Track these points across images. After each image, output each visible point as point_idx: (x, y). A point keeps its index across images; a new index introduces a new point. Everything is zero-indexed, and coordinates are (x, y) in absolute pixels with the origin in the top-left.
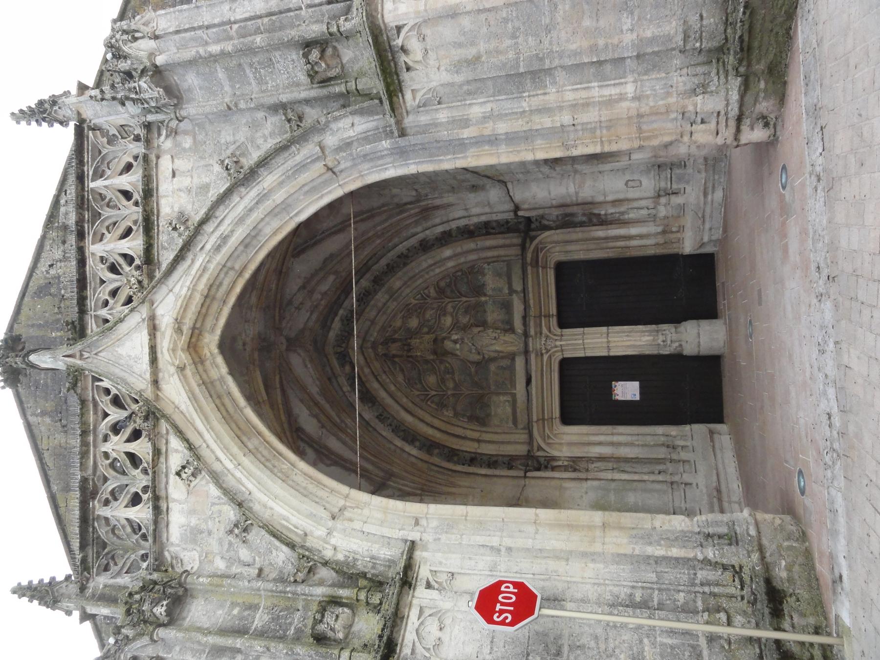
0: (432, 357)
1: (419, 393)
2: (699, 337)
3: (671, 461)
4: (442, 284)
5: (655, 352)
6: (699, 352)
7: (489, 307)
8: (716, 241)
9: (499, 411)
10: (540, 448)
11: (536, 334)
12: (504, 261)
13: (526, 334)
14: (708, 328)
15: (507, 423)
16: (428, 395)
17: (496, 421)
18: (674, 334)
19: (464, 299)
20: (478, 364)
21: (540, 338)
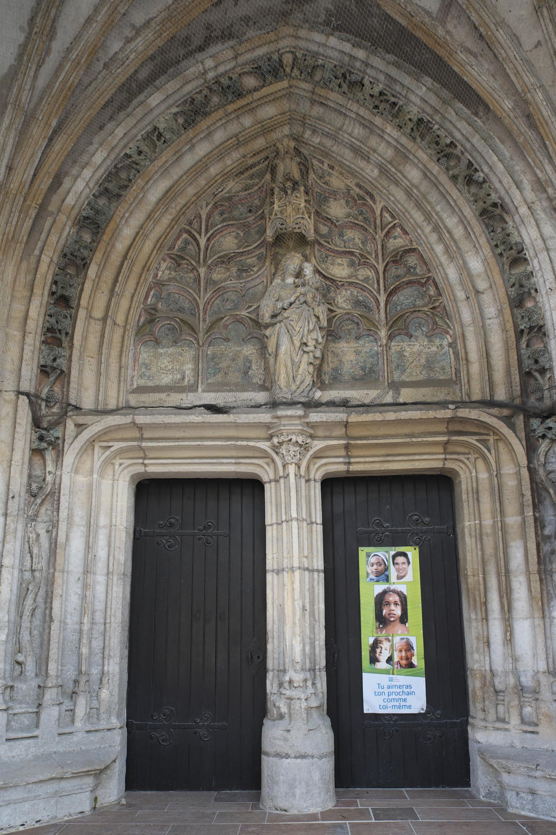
1: (204, 217)
2: (296, 757)
5: (270, 664)
6: (267, 754)
8: (502, 796)
10: (80, 427)
11: (312, 425)
12: (458, 371)
14: (316, 776)
16: (200, 235)
17: (145, 355)
18: (304, 705)
19: (382, 299)
21: (302, 433)
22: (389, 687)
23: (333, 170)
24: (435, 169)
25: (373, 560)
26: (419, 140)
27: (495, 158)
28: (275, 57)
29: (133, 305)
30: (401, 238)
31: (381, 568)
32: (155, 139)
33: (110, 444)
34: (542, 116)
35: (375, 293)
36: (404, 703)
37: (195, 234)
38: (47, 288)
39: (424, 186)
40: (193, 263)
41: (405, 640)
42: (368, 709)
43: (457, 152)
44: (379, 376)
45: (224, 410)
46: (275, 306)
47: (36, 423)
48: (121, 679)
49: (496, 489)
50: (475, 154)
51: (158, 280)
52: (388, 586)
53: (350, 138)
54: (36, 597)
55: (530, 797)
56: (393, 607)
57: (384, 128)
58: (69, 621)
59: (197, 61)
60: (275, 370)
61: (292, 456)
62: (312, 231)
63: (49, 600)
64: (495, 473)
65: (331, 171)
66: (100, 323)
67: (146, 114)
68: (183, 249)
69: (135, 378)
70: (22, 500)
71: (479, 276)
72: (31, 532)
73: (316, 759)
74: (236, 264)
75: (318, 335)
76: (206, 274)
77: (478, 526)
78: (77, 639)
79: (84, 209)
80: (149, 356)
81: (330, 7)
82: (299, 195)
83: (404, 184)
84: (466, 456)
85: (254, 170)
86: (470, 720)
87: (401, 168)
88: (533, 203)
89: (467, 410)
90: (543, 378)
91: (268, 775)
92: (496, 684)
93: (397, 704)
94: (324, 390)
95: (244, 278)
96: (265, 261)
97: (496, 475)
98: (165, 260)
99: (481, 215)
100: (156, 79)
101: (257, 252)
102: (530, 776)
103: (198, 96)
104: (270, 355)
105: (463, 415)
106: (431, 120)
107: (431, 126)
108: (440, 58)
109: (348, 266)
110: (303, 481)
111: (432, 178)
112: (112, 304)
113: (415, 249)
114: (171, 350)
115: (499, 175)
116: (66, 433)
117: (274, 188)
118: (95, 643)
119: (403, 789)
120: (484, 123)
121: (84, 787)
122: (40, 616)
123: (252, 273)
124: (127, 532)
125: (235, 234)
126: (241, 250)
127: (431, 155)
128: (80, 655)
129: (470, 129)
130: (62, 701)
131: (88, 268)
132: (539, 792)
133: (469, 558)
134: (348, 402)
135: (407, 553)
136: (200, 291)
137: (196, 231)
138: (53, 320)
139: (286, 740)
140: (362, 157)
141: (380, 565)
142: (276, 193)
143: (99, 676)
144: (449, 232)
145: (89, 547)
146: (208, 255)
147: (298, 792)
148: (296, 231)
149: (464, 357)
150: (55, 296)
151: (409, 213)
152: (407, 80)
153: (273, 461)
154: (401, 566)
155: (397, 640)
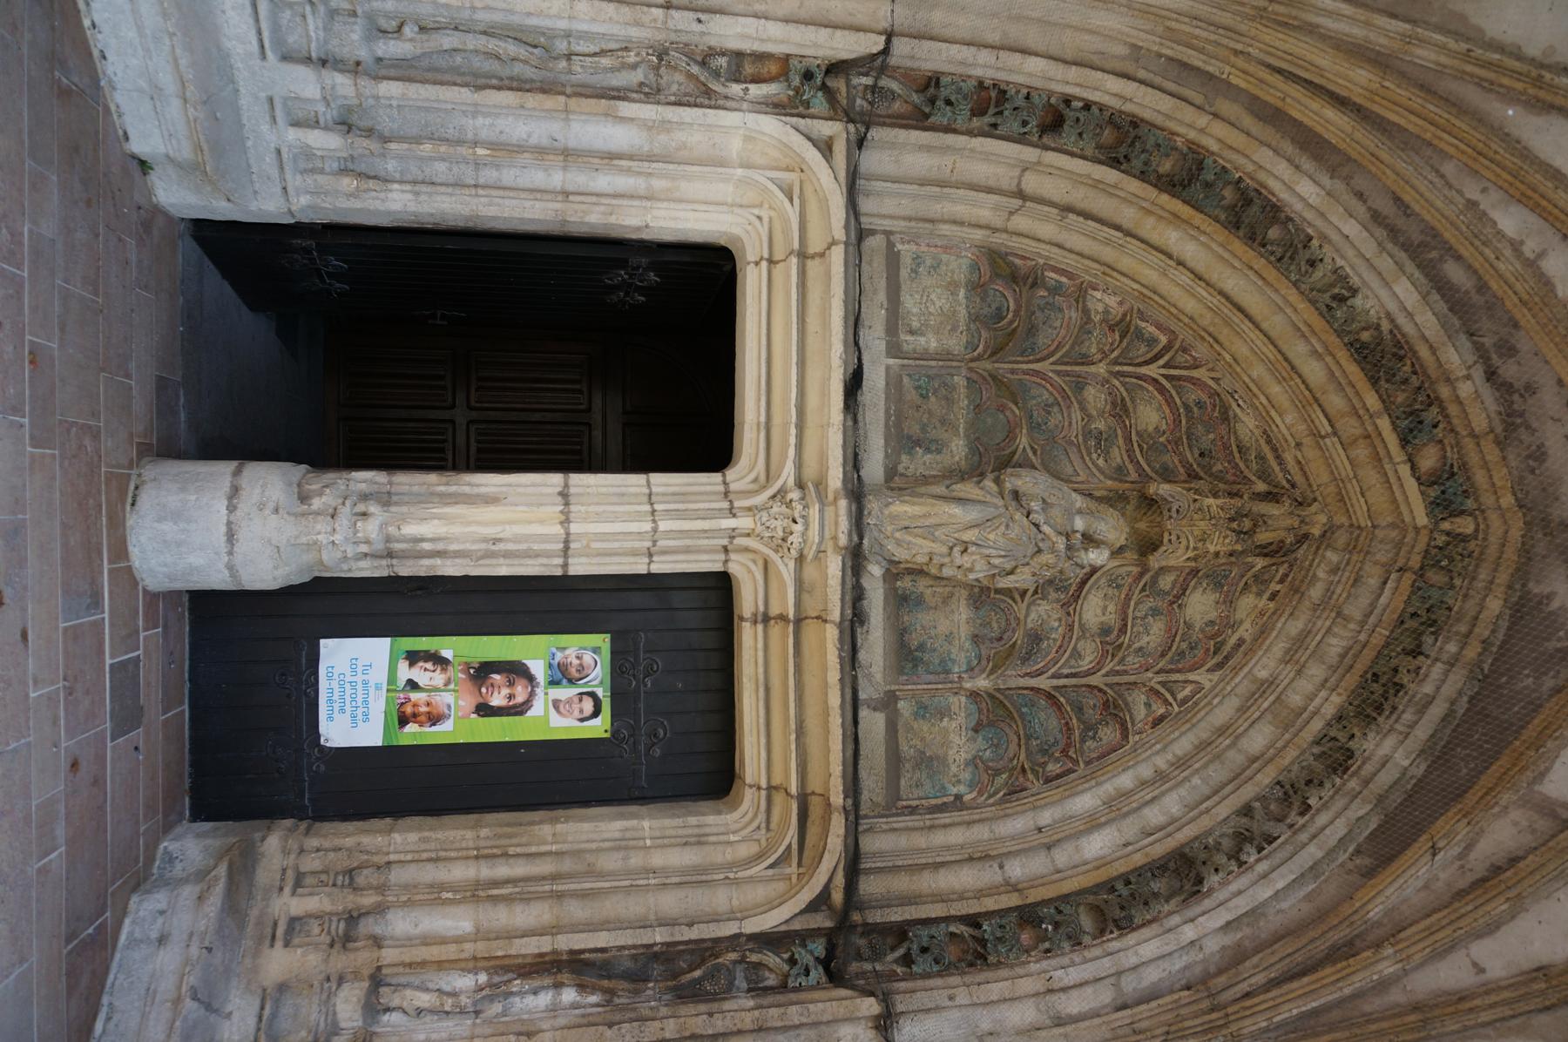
0: (1164, 489)
1: (1195, 373)
2: (229, 523)
3: (356, 68)
4: (1108, 734)
6: (237, 473)
7: (961, 653)
9: (940, 301)
10: (826, 147)
12: (913, 810)
13: (856, 559)
14: (197, 560)
15: (917, 259)
16: (1164, 367)
19: (1043, 683)
20: (1005, 463)
22: (365, 683)
23: (1269, 599)
24: (1266, 778)
25: (588, 658)
26: (1316, 750)
27: (1280, 885)
28: (1470, 504)
29: (1044, 246)
30: (1147, 716)
31: (574, 673)
32: (1336, 291)
33: (796, 201)
34: (1354, 973)
35: (1053, 670)
36: (336, 709)
37: (1166, 358)
38: (1076, 91)
39: (1235, 758)
40: (1115, 354)
41: (446, 711)
42: (327, 646)
43: (1293, 817)
44: (907, 674)
46: (1033, 497)
47: (837, 68)
48: (377, 212)
49: (704, 878)
50: (1289, 848)
51: (1086, 291)
52: (542, 683)
53: (1323, 631)
54: (521, 61)
55: (154, 935)
56: (505, 691)
57: (1339, 690)
58: (480, 121)
59: (1470, 367)
60: (922, 495)
61: (768, 524)
62: (1164, 563)
63: (515, 84)
64: (731, 875)
65: (1266, 595)
66: (1013, 187)
67: (1380, 274)
68: (1139, 334)
69: (914, 247)
70: (696, 39)
71: (1077, 849)
72: (638, 54)
73: (226, 559)
74: (1110, 428)
75: (980, 573)
76: (1095, 376)
77: (641, 843)
78: (447, 136)
79: (1215, 162)
80: (953, 272)
81: (1555, 604)
82: (1227, 541)
83: (1240, 721)
84: (763, 825)
85: (1273, 463)
86: (304, 825)
87: (1269, 717)
88: (1201, 948)
89: (842, 831)
90: (896, 961)
91: (199, 474)
92: (365, 872)
93: (336, 697)
94: (885, 581)
95: (1085, 441)
96: (1116, 479)
97: (727, 878)
98: (1121, 303)
99: (1183, 856)
100: (1439, 290)
101: (1130, 467)
102: (191, 935)
103: (1407, 368)
104: (947, 487)
105: (833, 822)
106: (1349, 772)
107: (1339, 772)
108: (1459, 795)
109: (1102, 623)
110: (725, 542)
111: (1248, 773)
112: (1046, 209)
113: (1127, 737)
114: (962, 313)
115: (1251, 891)
116: (815, 121)
117: (1241, 497)
118: (441, 167)
119: (186, 707)
120: (1342, 865)
121: (174, 142)
122: (488, 68)
123: (1094, 456)
124: (639, 229)
125: (1164, 427)
126: (1134, 438)
127: (1290, 771)
128: (417, 140)
129: (1332, 842)
130: (333, 105)
131: (1111, 167)
132: (162, 952)
133: (586, 826)
134: (862, 623)
135: (600, 717)
136: (1066, 364)
137: (1172, 358)
138: (1020, 101)
139: (261, 507)
140: (1290, 649)
141: (578, 671)
142: (1232, 501)
143: (382, 174)
144: (1154, 799)
145: (610, 159)
146: (1127, 380)
147: (167, 527)
148: (1166, 535)
149: (937, 822)
150: (1062, 106)
151: (1189, 729)
152: (1422, 733)
153: (764, 488)
154: (576, 706)
155: (448, 698)
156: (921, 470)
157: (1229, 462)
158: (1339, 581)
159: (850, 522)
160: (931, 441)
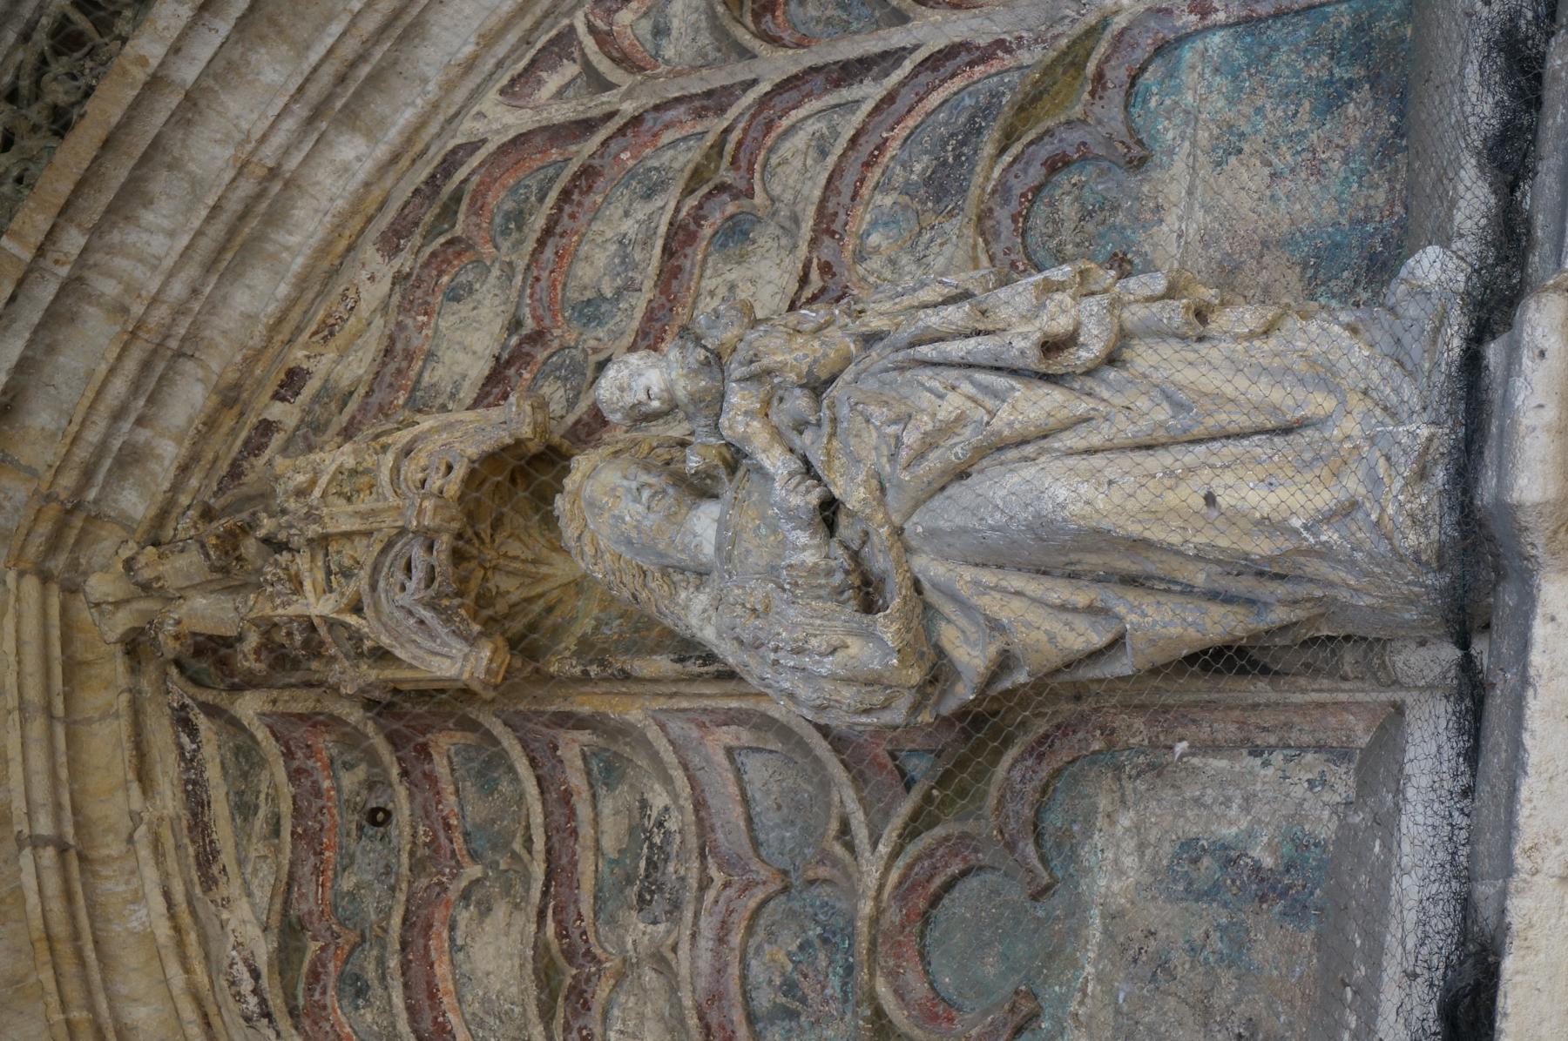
45: (1469, 975)
65: (311, 387)
74: (612, 921)
109: (741, 259)
125: (464, 916)
126: (538, 870)
156: (1265, 774)
157: (317, 793)
158: (117, 416)
159: (1507, 401)
160: (1212, 893)
